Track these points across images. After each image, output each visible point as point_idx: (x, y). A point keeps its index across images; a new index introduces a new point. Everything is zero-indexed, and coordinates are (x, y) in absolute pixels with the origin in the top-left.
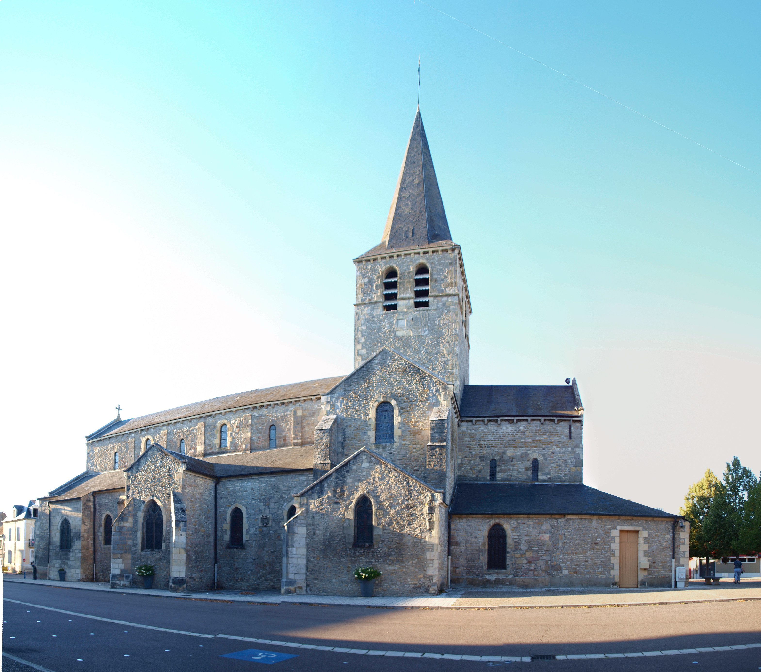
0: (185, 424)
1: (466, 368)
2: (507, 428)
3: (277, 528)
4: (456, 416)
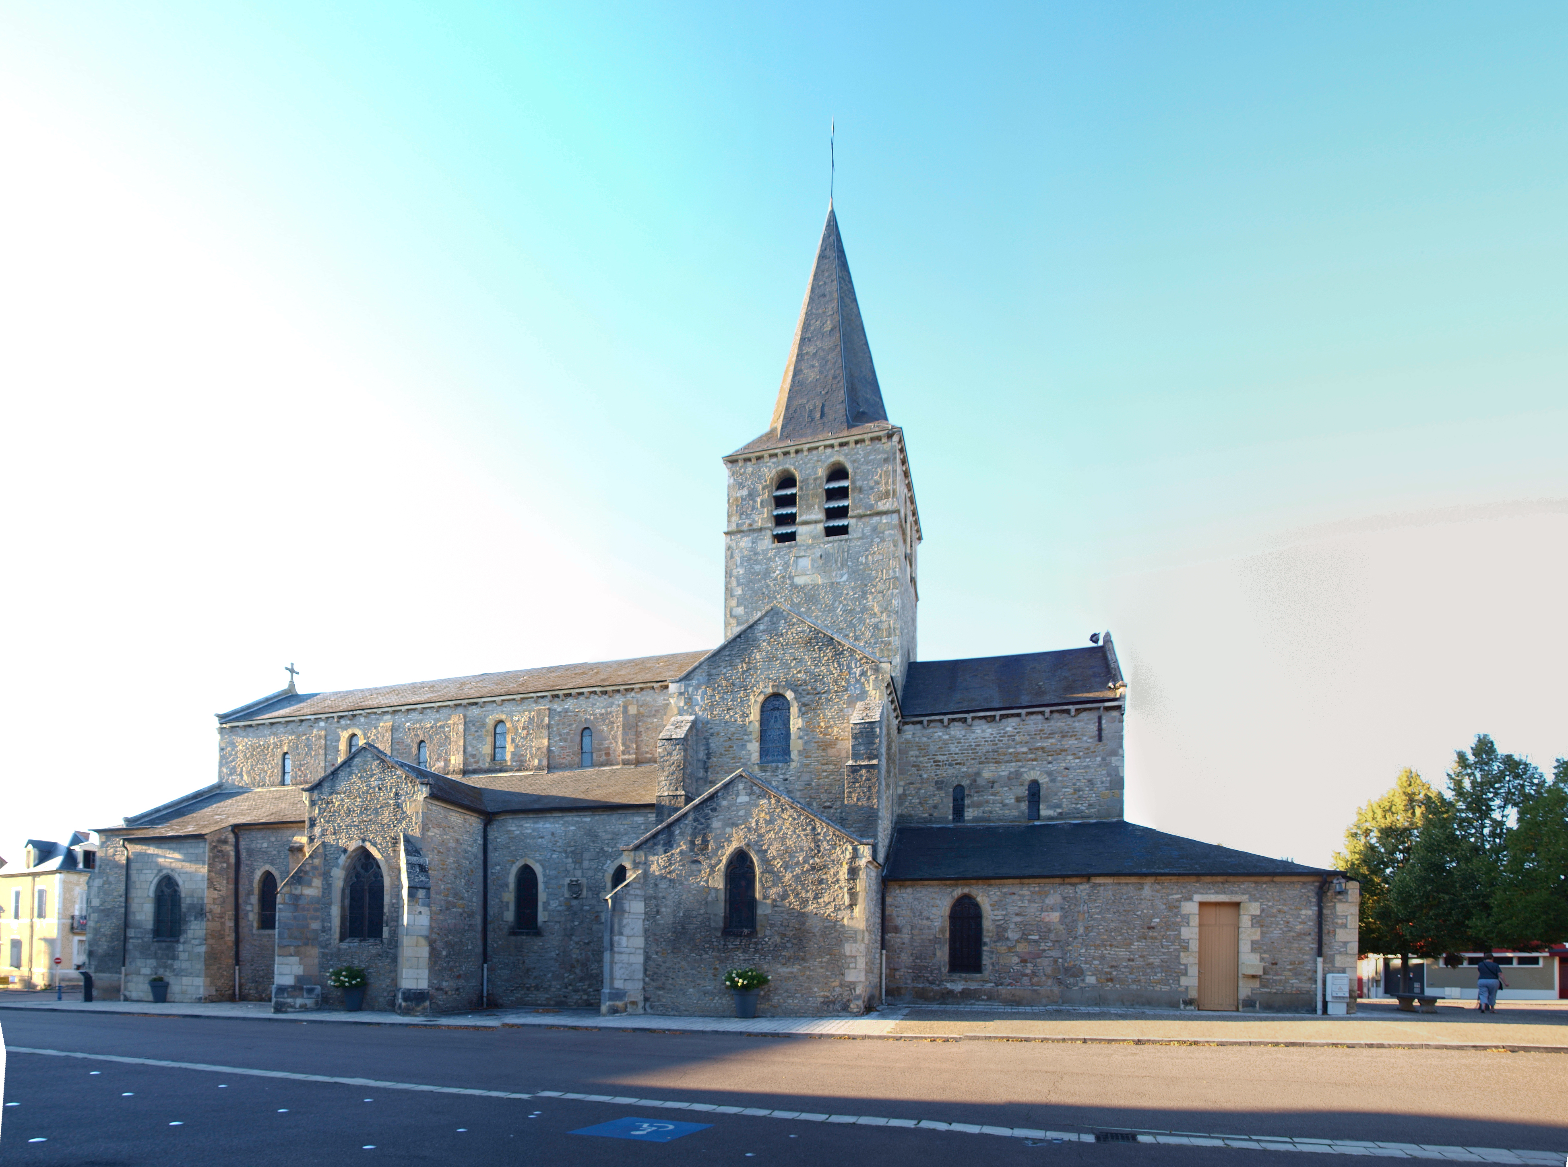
0: (426, 714)
1: (911, 634)
2: (983, 731)
3: (594, 902)
4: (895, 715)
